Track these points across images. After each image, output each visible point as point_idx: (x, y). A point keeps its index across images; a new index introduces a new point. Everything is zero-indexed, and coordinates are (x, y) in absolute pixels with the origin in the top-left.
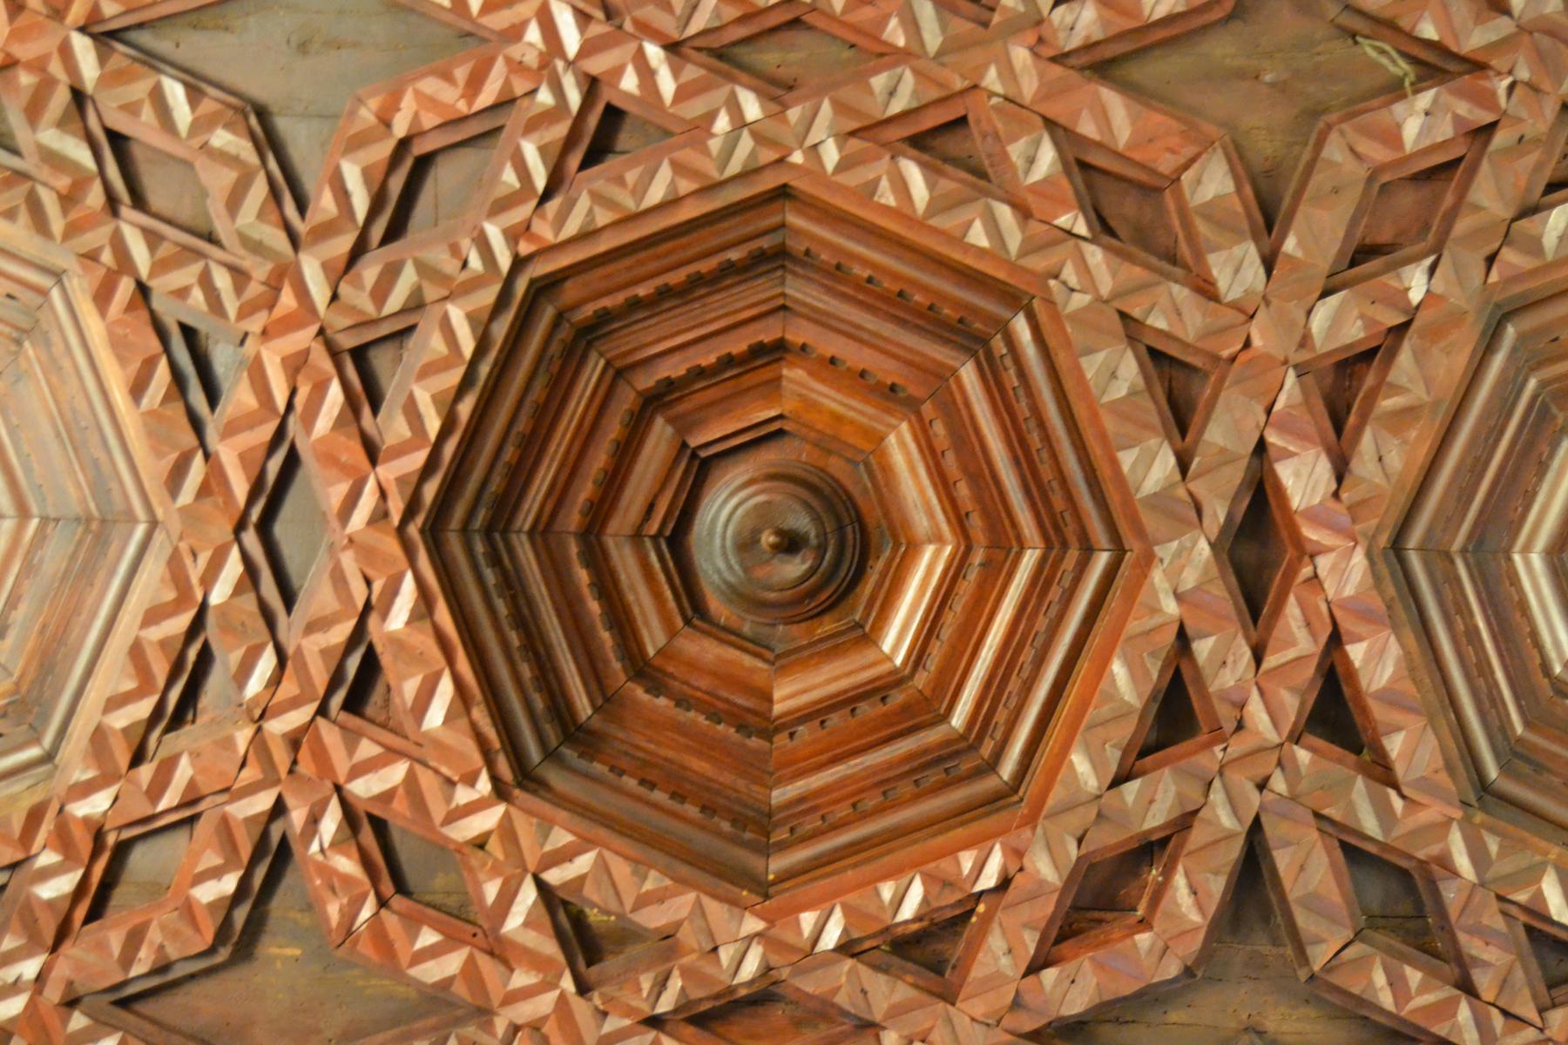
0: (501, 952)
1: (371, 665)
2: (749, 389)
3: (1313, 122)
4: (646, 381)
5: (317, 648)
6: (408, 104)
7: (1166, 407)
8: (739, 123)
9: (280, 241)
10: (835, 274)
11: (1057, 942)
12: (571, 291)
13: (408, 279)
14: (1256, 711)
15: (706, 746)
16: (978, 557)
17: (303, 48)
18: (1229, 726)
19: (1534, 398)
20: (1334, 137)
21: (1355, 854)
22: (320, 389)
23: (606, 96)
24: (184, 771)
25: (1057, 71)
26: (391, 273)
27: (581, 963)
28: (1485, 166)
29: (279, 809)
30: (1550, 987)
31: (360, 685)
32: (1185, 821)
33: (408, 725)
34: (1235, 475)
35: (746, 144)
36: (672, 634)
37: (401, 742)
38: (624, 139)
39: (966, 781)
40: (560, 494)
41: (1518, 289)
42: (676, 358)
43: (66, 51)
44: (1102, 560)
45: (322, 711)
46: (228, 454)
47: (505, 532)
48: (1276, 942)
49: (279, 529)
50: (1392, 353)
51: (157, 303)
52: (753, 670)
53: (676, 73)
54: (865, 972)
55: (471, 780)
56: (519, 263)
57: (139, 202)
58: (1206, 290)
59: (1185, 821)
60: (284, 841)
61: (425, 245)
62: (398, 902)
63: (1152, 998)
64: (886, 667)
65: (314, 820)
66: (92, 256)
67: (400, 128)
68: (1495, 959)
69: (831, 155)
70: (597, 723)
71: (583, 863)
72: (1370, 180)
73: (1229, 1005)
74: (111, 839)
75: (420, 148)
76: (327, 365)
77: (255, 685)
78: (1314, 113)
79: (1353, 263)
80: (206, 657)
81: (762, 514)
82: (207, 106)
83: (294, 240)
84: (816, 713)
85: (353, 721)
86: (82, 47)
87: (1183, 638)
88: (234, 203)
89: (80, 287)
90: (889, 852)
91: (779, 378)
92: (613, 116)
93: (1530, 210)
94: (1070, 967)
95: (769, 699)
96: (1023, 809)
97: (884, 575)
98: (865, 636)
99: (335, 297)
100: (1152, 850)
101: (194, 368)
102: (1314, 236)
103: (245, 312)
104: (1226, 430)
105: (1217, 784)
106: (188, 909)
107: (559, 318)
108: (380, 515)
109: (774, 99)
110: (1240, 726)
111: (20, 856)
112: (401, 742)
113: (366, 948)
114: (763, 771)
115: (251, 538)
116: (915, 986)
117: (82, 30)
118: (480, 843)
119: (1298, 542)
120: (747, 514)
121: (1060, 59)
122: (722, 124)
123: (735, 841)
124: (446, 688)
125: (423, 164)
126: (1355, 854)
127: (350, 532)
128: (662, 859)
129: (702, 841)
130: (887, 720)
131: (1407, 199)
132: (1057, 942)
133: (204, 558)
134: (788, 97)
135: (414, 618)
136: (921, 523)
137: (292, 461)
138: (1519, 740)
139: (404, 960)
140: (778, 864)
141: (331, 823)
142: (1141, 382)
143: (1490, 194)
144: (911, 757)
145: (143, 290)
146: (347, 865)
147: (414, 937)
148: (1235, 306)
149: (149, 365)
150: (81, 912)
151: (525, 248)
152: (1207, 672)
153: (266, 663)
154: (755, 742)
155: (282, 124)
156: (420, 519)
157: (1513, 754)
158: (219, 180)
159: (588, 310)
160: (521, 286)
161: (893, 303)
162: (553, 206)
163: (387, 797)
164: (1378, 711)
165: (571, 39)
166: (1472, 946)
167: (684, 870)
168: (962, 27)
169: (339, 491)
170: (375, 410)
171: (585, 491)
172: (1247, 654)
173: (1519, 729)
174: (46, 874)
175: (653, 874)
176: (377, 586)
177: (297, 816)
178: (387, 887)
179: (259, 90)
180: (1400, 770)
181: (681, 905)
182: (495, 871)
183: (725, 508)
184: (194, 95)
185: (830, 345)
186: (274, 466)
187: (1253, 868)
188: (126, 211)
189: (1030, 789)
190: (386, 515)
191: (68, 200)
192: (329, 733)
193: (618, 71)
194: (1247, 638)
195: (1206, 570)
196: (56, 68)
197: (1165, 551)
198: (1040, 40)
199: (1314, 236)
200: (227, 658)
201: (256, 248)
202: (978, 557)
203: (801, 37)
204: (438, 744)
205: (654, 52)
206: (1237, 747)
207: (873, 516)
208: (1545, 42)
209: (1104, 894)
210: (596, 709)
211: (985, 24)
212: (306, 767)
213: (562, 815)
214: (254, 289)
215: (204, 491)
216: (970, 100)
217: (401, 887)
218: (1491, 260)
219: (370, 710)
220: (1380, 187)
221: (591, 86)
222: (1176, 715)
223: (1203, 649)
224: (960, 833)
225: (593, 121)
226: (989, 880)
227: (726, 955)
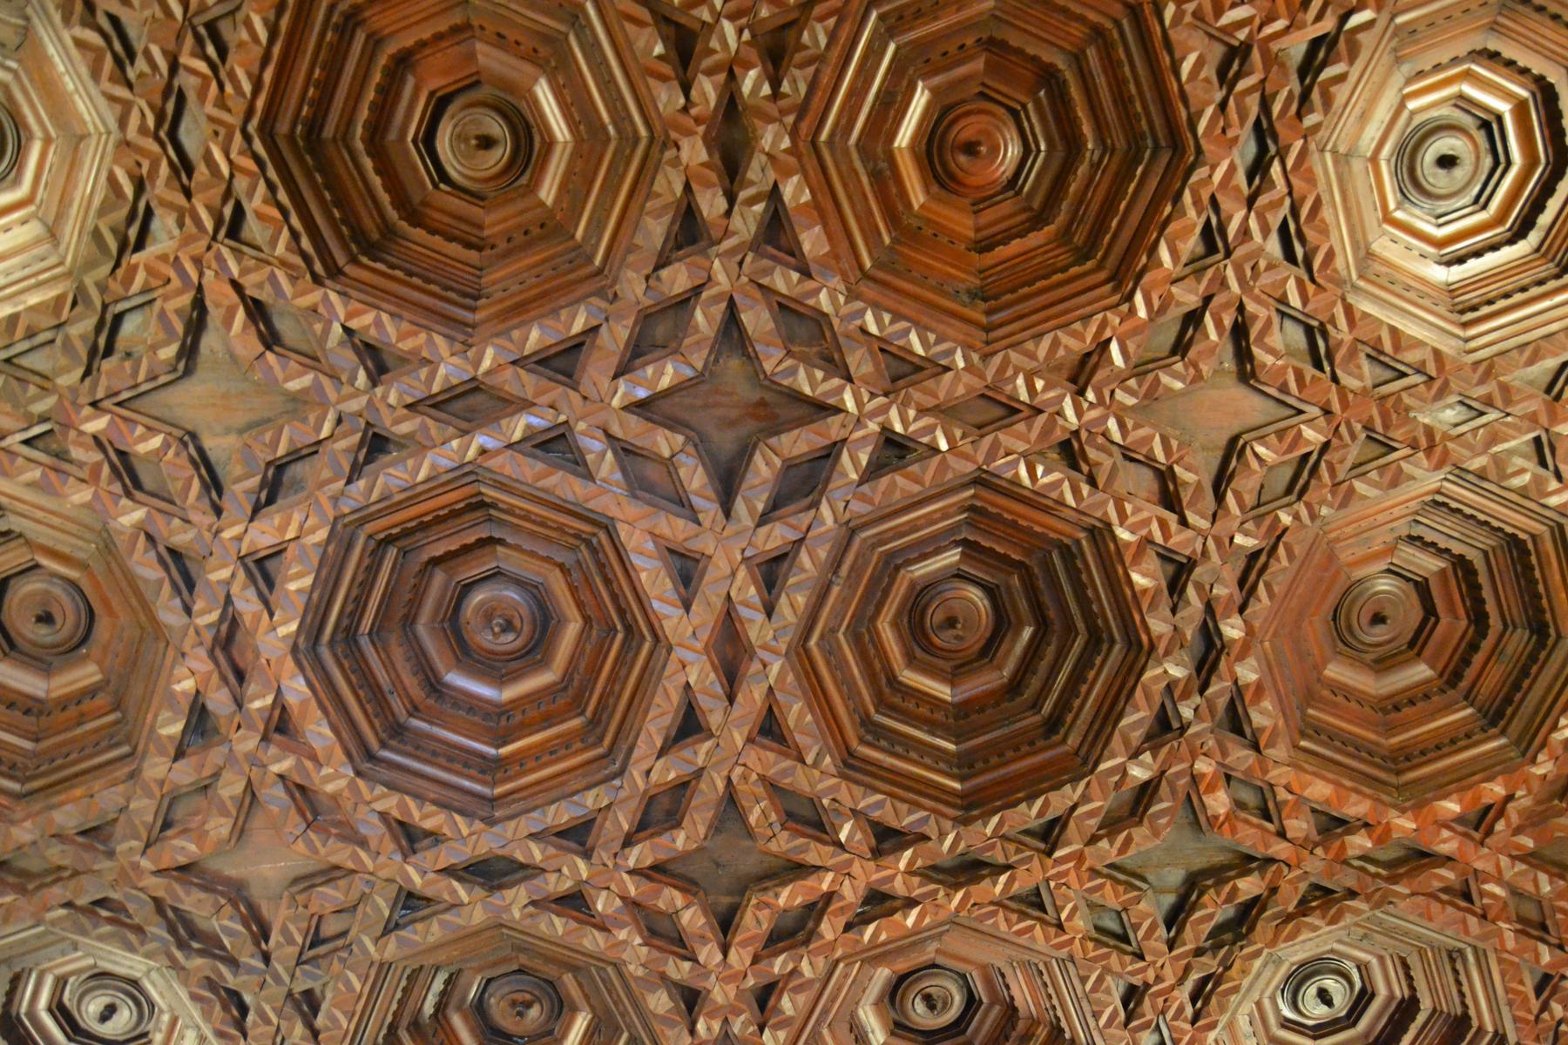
91: (978, 230)
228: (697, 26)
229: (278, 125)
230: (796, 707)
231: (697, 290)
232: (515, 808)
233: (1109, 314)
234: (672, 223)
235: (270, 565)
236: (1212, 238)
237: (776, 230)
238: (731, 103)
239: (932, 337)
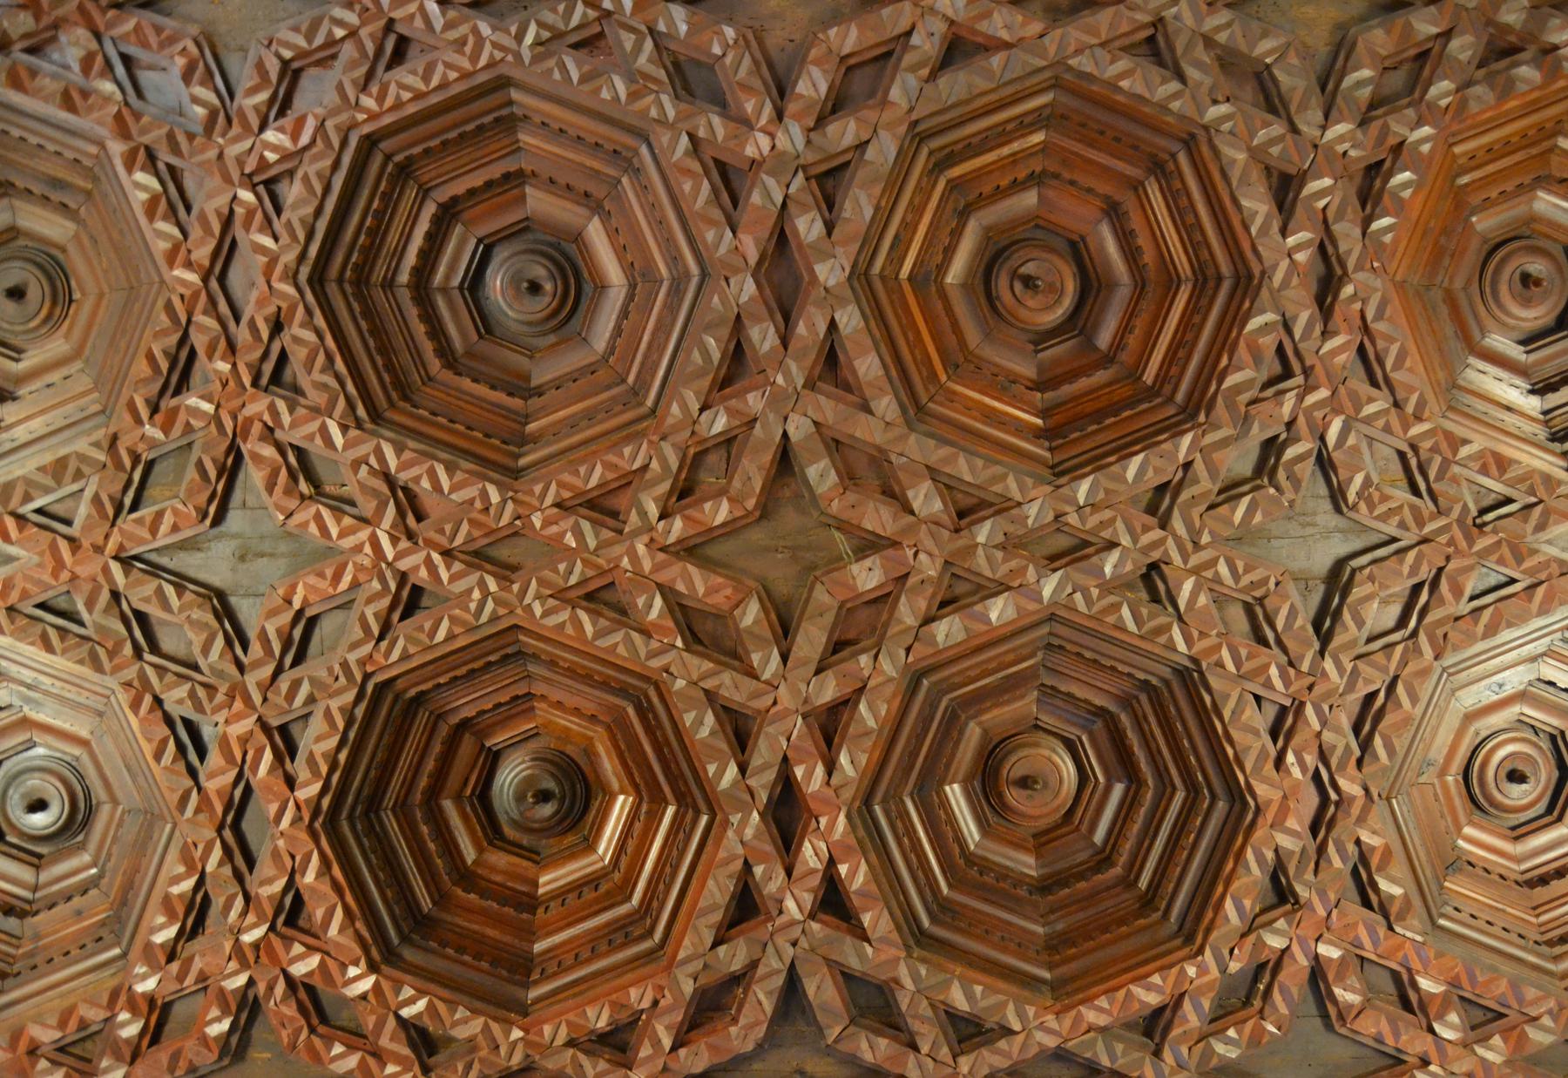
0: (379, 1056)
1: (298, 901)
2: (518, 714)
3: (810, 573)
4: (454, 720)
5: (270, 888)
6: (300, 590)
7: (733, 739)
8: (486, 593)
9: (232, 670)
10: (552, 663)
11: (688, 1031)
12: (400, 684)
13: (305, 689)
14: (790, 904)
15: (499, 921)
16: (644, 808)
17: (242, 558)
18: (775, 913)
19: (946, 708)
20: (818, 586)
21: (848, 978)
22: (260, 752)
23: (412, 580)
24: (198, 964)
25: (661, 556)
26: (295, 685)
27: (425, 1057)
28: (903, 599)
29: (251, 982)
30: (960, 1042)
31: (291, 914)
32: (753, 965)
33: (321, 935)
34: (770, 775)
35: (490, 605)
36: (480, 850)
37: (314, 940)
38: (425, 602)
39: (637, 935)
40: (409, 785)
41: (925, 664)
42: (471, 706)
43: (106, 570)
44: (704, 819)
45: (272, 928)
46: (211, 786)
47: (377, 813)
48: (808, 1024)
49: (245, 825)
50: (857, 702)
51: (167, 707)
52: (526, 869)
53: (448, 568)
54: (582, 1057)
55: (356, 963)
56: (367, 677)
57: (155, 648)
58: (752, 674)
59: (753, 965)
60: (256, 997)
61: (315, 667)
62: (322, 1029)
63: (740, 1060)
64: (600, 865)
65: (271, 988)
66: (128, 684)
67: (297, 605)
68: (928, 1035)
69: (538, 610)
70: (436, 913)
71: (421, 1004)
72: (840, 608)
73: (789, 1058)
74: (159, 1002)
75: (309, 613)
76: (263, 739)
77: (233, 915)
78: (814, 567)
79: (835, 652)
80: (206, 900)
81: (528, 782)
82: (188, 596)
83: (241, 667)
84: (561, 894)
85: (289, 932)
86: (115, 568)
87: (747, 866)
88: (206, 650)
89: (123, 698)
90: (593, 987)
91: (533, 708)
92: (417, 591)
93: (928, 620)
94: (693, 1047)
95: (536, 885)
96: (664, 962)
97: (598, 811)
98: (589, 845)
99: (265, 699)
100: (740, 979)
101: (190, 741)
102: (811, 639)
103: (215, 711)
104: (764, 753)
105: (770, 945)
106: (204, 1040)
107: (397, 697)
108: (297, 820)
109: (505, 578)
110: (781, 912)
111: (108, 1014)
112: (314, 940)
113: (304, 1056)
114: (531, 934)
115: (227, 833)
116: (609, 1061)
117: (116, 558)
118: (364, 997)
119: (809, 810)
120: (520, 782)
121: (663, 549)
122: (476, 595)
123: (508, 981)
124: (339, 913)
125: (313, 622)
126: (848, 978)
127: (280, 827)
128: (466, 999)
129: (488, 981)
130: (597, 901)
131: (864, 615)
132: (688, 1031)
133: (201, 847)
134: (513, 577)
135: (319, 875)
136: (615, 785)
137: (248, 791)
138: (946, 899)
139: (326, 1061)
140: (533, 994)
141: (280, 987)
142: (717, 727)
143: (907, 612)
144: (608, 924)
145: (158, 701)
146: (290, 1010)
147: (329, 1049)
148: (767, 682)
149: (164, 742)
150: (145, 1042)
151: (369, 669)
152: (761, 885)
153: (239, 902)
154: (525, 916)
155: (233, 600)
156: (321, 820)
157: (942, 909)
158: (197, 639)
159: (412, 692)
160: (370, 688)
161: (587, 678)
162: (384, 644)
163: (310, 974)
164: (856, 901)
165: (390, 553)
166: (915, 1025)
167: (478, 1005)
168: (607, 534)
169: (273, 808)
170: (292, 761)
171: (423, 782)
172: (782, 874)
173: (945, 890)
174: (124, 1025)
175: (461, 1008)
176: (298, 859)
177: (261, 987)
178: (315, 1021)
179: (216, 581)
180: (869, 933)
181: (477, 1025)
182: (372, 1012)
183: (510, 775)
184: (180, 590)
185: (556, 695)
186: (238, 793)
187: (792, 987)
188: (148, 657)
189: (669, 949)
190: (301, 819)
191: (112, 654)
192: (276, 942)
193: (417, 568)
194: (783, 863)
195: (757, 829)
196: (101, 579)
197: (735, 819)
198: (652, 540)
199: (811, 639)
200: (218, 902)
201: (220, 674)
202: (644, 808)
203: (521, 541)
204: (337, 945)
205: (436, 557)
206: (779, 921)
207: (591, 777)
208: (933, 527)
209: (711, 1005)
210: (434, 903)
211: (620, 532)
212: (264, 959)
213: (408, 978)
214: (220, 697)
215: (197, 811)
216: (615, 573)
217: (324, 1020)
218: (908, 650)
219: (301, 923)
220: (846, 612)
221: (403, 577)
222: (746, 906)
223: (758, 870)
224: (630, 976)
225: (405, 593)
226: (646, 1004)
227: (503, 1051)
228: (821, 916)
229: (1227, 808)
230: (704, 732)
231: (821, 121)
232: (1035, 80)
233: (384, 663)
234: (848, 725)
235: (1271, 898)
236: (285, 742)
237: (740, 732)
238: (786, 314)
239: (569, 630)
